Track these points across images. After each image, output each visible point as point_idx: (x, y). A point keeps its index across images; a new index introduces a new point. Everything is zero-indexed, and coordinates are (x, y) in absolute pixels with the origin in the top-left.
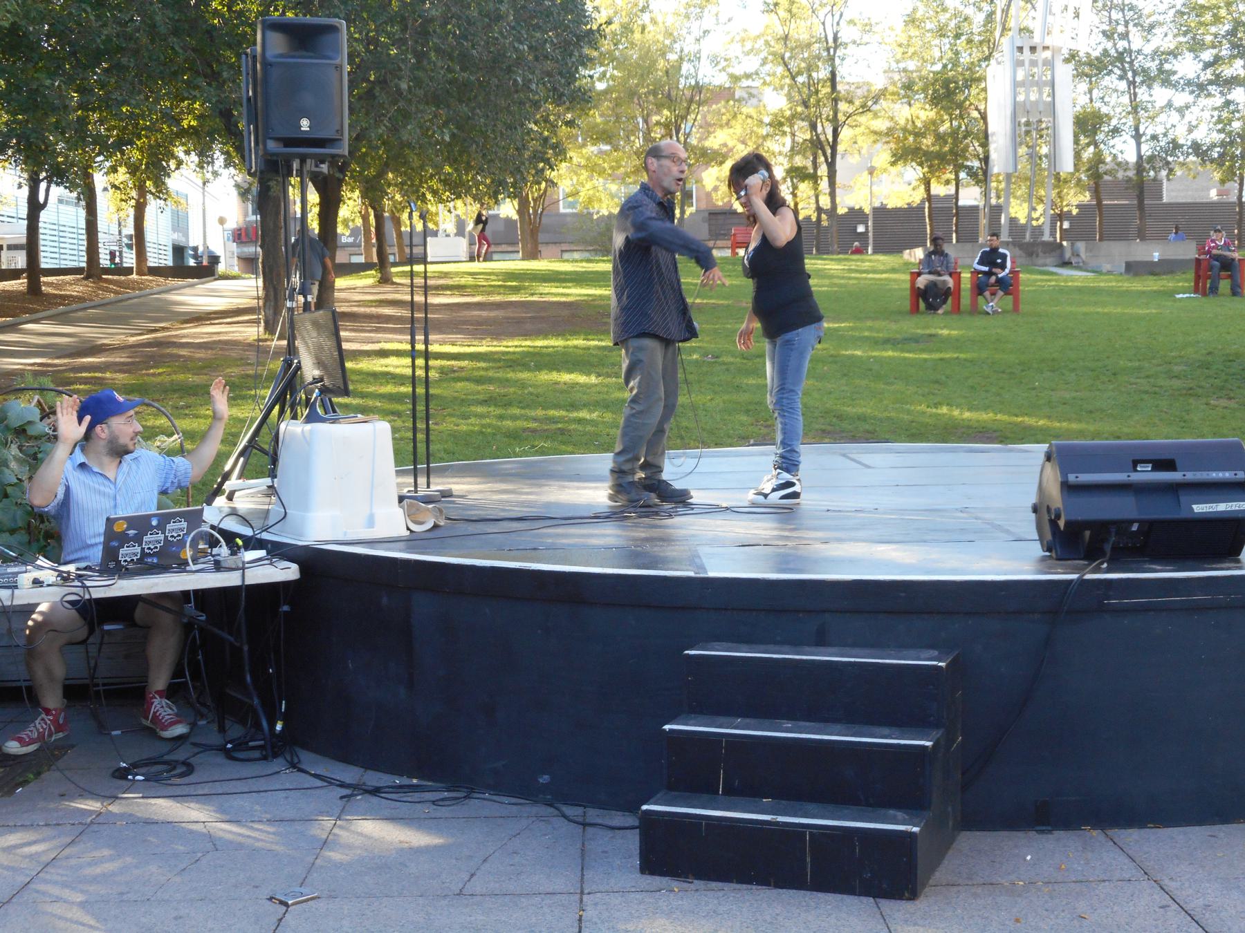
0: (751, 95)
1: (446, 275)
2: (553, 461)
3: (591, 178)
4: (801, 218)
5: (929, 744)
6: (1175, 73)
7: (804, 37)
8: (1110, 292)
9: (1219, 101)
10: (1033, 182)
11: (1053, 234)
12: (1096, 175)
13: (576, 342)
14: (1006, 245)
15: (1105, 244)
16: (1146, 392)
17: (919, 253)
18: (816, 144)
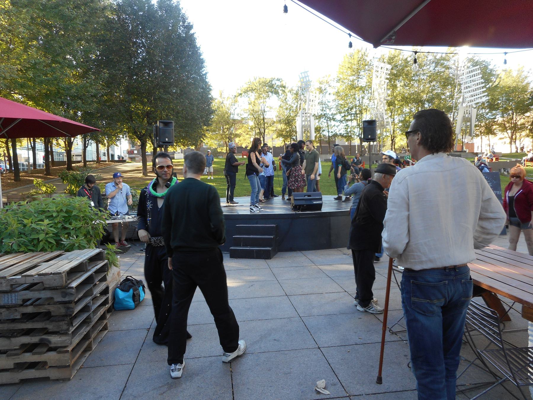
9: (345, 124)
18: (260, 133)
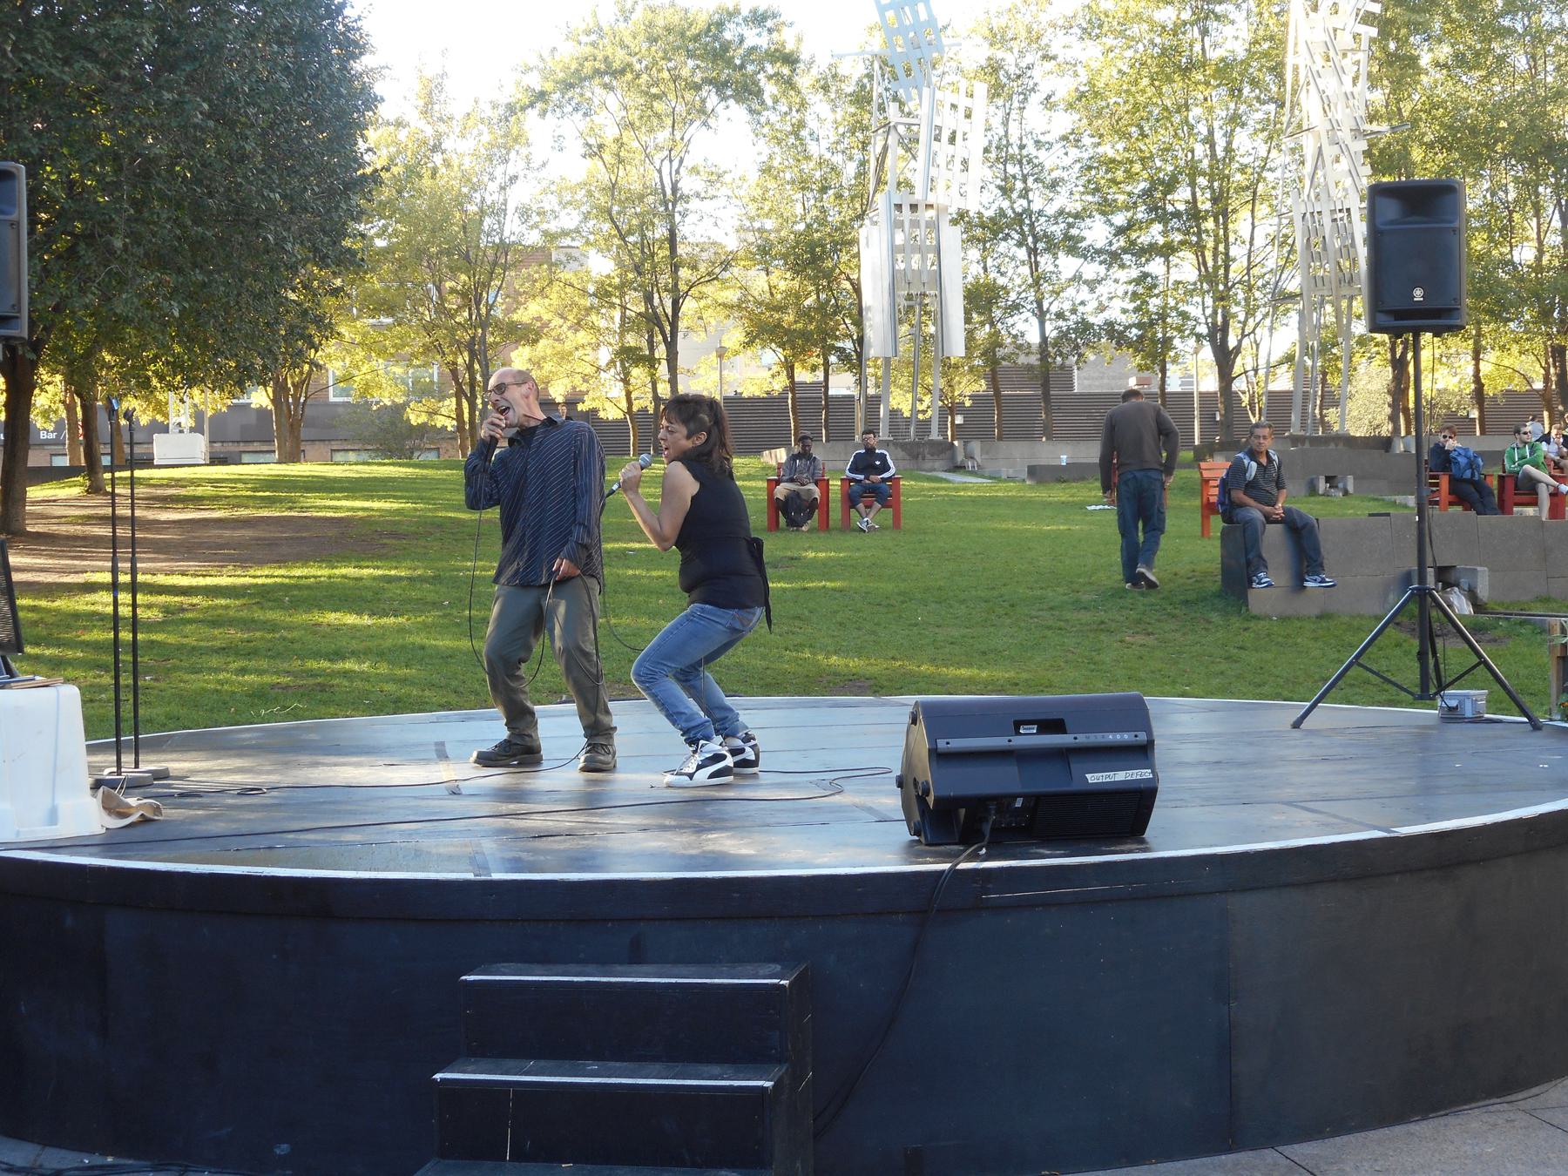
0: (570, 257)
1: (178, 483)
2: (309, 729)
3: (369, 358)
4: (635, 409)
5: (769, 1084)
6: (1084, 239)
7: (637, 187)
8: (1008, 502)
9: (1134, 273)
10: (916, 369)
11: (942, 430)
12: (993, 360)
13: (344, 571)
14: (886, 444)
15: (1003, 444)
16: (1049, 628)
17: (781, 455)
18: (652, 320)
